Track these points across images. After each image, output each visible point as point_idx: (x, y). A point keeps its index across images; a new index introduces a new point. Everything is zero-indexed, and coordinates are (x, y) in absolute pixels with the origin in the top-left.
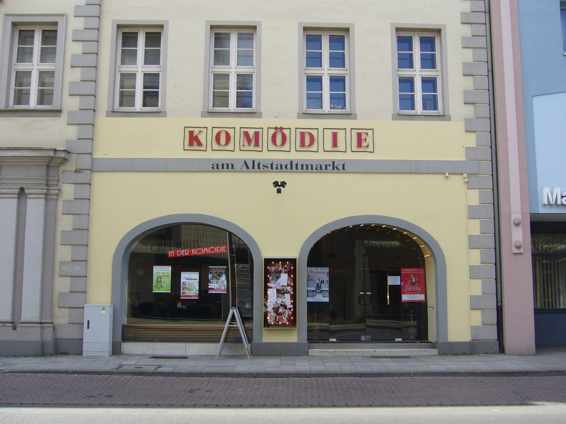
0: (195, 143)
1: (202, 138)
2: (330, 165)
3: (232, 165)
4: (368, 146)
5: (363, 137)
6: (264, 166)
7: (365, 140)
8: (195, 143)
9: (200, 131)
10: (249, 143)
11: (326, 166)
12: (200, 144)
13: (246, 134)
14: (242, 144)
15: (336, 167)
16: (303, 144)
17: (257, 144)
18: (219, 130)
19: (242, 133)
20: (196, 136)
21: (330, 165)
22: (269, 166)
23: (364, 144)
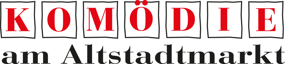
0: (16, 26)
1: (27, 19)
2: (250, 53)
3: (45, 55)
4: (274, 30)
5: (267, 15)
6: (111, 56)
7: (271, 19)
8: (16, 26)
9: (24, 9)
10: (98, 24)
11: (242, 55)
12: (23, 28)
13: (93, 11)
14: (86, 28)
15: (264, 58)
16: (177, 27)
17: (109, 27)
18: (65, 33)
19: (87, 11)
20: (19, 17)
21: (250, 53)
22: (123, 57)
23: (268, 25)
